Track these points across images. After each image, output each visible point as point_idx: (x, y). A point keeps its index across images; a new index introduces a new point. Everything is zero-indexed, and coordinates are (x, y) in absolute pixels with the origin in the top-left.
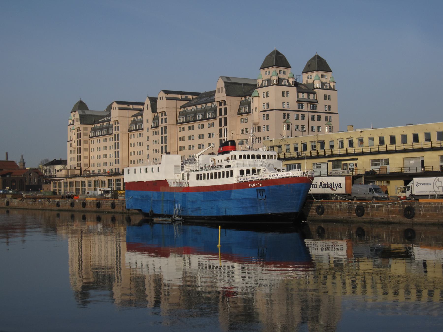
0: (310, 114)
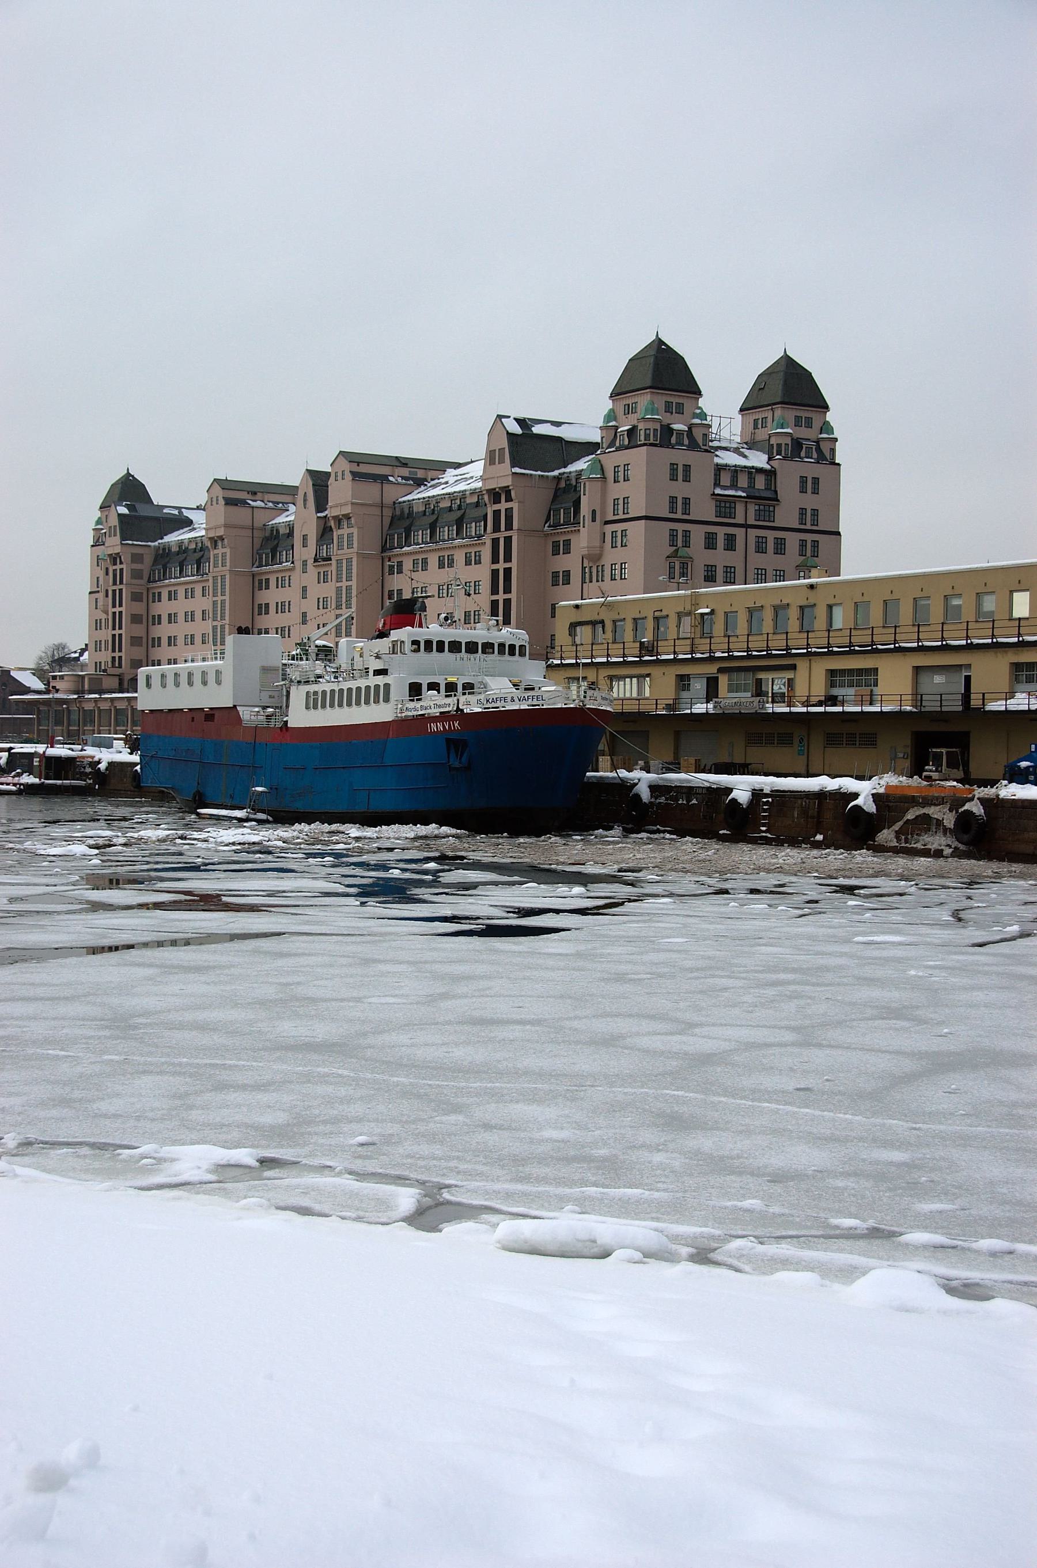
0: (753, 533)
